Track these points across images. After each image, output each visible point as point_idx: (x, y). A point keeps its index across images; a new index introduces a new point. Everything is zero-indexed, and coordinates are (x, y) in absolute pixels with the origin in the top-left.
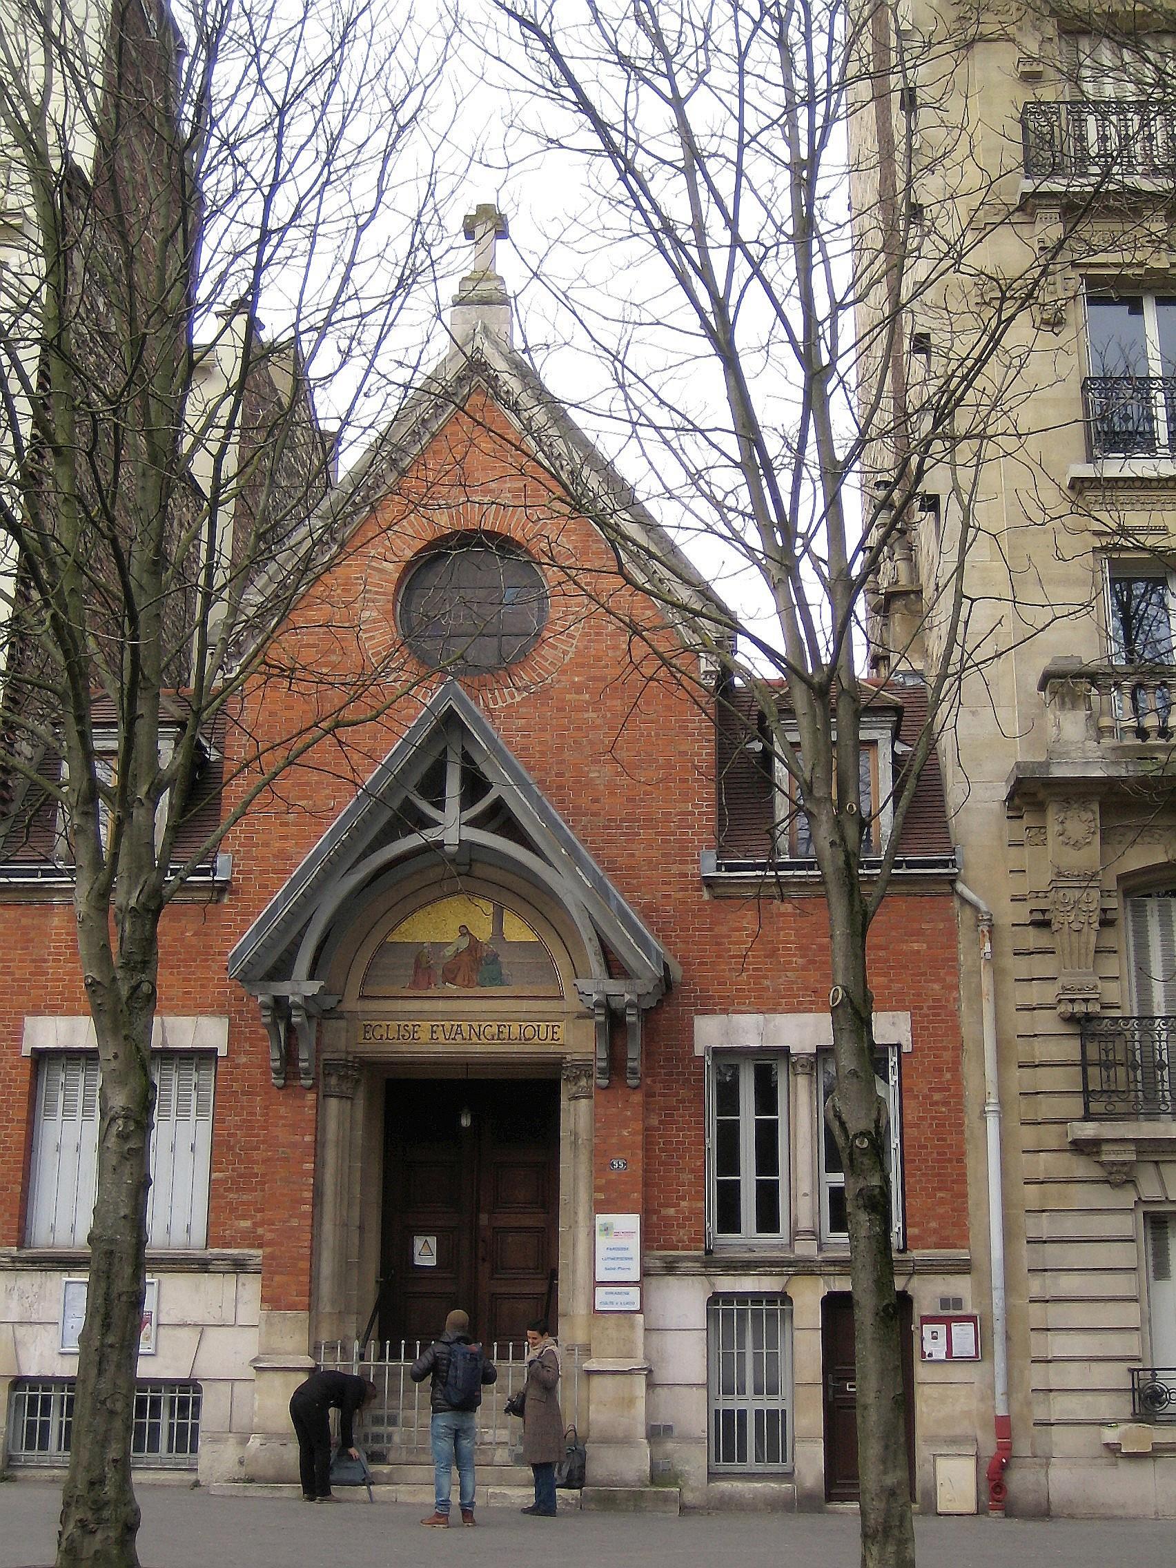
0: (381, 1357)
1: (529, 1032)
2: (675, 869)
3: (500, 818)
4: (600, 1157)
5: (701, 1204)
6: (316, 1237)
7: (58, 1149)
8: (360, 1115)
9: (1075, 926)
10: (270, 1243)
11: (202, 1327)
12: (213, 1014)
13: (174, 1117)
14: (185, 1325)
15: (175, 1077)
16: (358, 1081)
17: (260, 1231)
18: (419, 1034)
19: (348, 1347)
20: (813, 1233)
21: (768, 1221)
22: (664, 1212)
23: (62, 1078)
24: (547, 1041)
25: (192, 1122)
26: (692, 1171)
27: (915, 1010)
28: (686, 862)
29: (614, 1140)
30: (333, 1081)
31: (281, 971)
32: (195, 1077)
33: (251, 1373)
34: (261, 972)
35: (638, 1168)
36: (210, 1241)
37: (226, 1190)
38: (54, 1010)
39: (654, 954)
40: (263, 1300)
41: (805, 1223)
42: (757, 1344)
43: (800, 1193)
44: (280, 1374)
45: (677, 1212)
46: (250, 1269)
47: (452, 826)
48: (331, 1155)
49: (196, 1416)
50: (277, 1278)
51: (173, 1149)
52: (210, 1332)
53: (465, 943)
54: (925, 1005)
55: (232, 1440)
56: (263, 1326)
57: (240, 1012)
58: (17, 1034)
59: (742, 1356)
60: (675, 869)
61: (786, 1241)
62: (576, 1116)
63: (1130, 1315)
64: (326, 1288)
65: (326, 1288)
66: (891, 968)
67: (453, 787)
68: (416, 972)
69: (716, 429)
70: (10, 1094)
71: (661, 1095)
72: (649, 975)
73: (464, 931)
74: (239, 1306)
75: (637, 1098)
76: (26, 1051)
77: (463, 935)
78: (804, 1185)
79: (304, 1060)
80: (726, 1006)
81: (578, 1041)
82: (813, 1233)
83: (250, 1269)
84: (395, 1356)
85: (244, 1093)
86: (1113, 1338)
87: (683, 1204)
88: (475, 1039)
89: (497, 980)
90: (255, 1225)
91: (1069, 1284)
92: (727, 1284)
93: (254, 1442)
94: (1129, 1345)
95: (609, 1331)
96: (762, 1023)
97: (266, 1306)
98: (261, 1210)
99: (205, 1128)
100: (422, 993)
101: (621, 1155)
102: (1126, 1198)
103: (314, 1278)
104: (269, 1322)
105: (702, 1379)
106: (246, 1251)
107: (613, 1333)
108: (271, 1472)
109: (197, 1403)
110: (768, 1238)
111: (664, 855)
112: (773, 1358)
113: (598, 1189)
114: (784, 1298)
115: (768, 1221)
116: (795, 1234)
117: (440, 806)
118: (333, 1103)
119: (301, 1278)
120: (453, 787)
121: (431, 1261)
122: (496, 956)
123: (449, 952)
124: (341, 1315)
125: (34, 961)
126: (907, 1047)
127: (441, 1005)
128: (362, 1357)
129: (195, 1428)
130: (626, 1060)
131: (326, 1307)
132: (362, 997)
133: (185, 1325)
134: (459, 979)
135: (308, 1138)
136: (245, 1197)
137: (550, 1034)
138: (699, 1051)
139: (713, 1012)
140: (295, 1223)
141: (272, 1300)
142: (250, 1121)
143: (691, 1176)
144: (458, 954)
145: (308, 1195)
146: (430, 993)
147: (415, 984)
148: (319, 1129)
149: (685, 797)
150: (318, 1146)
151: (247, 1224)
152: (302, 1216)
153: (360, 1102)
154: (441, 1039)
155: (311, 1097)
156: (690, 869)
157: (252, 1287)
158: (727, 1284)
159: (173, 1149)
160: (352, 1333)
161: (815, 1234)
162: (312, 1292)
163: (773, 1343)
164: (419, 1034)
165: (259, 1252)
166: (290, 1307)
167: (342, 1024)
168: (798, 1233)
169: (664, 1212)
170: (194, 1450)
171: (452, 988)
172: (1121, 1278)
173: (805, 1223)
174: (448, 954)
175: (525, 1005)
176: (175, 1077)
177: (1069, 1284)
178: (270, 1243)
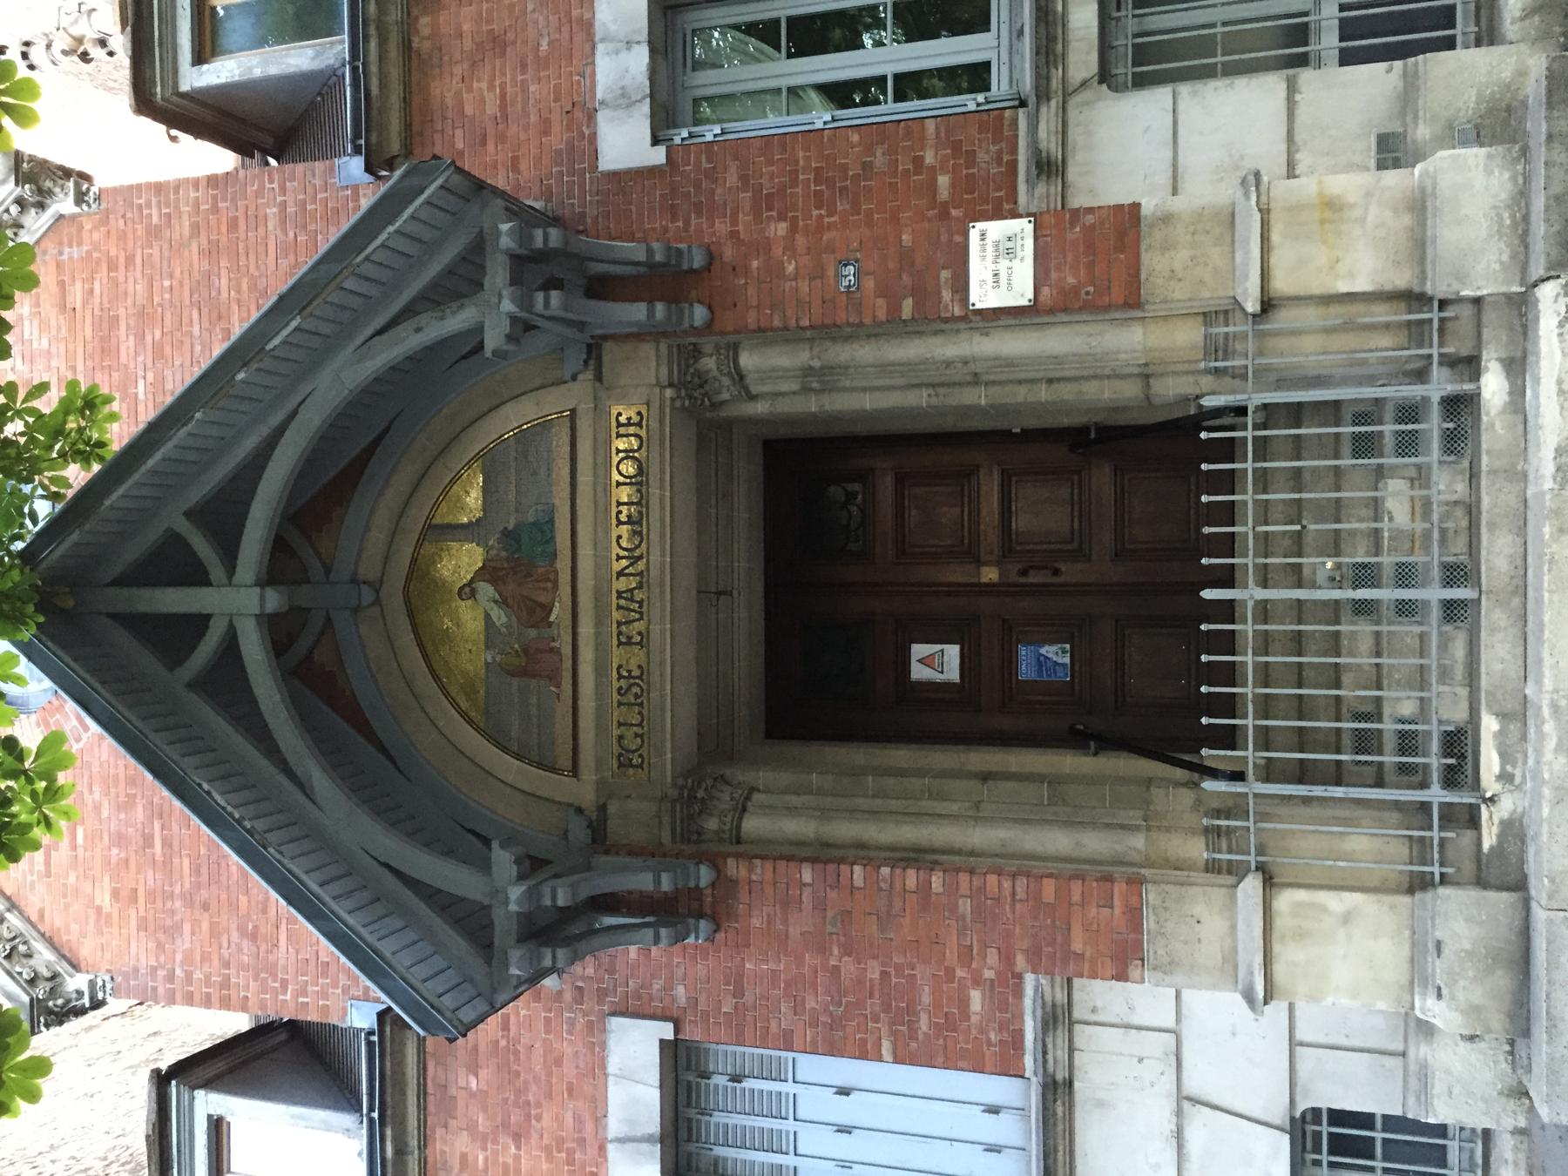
0: (1229, 738)
1: (629, 468)
3: (223, 516)
5: (930, 126)
8: (784, 778)
10: (1007, 958)
11: (1185, 1101)
12: (603, 1046)
13: (789, 1125)
14: (1179, 1135)
16: (723, 779)
17: (989, 974)
18: (633, 665)
19: (1215, 804)
24: (643, 433)
25: (798, 1089)
26: (869, 150)
29: (804, 287)
30: (712, 824)
31: (473, 923)
32: (720, 1080)
33: (1278, 1009)
34: (477, 966)
36: (1009, 1066)
37: (913, 1037)
39: (415, 181)
40: (1121, 976)
44: (1277, 948)
45: (944, 171)
46: (1061, 997)
47: (238, 602)
48: (845, 830)
49: (1365, 1120)
50: (1077, 946)
51: (845, 1130)
52: (1192, 1085)
53: (486, 590)
55: (1421, 1051)
56: (1179, 979)
57: (602, 994)
64: (1095, 843)
65: (1095, 843)
67: (175, 600)
68: (534, 676)
71: (734, 222)
74: (1136, 1021)
77: (473, 594)
79: (658, 881)
80: (581, 114)
83: (1061, 997)
84: (1229, 482)
85: (739, 992)
87: (929, 158)
88: (641, 565)
89: (544, 528)
90: (977, 981)
92: (1082, 58)
93: (1431, 1008)
95: (1178, 266)
96: (610, 46)
97: (1134, 972)
98: (950, 973)
99: (812, 1066)
100: (568, 664)
101: (831, 272)
103: (1074, 870)
104: (1168, 967)
106: (1028, 1002)
107: (1180, 258)
108: (1502, 980)
109: (1338, 1117)
117: (201, 622)
118: (753, 825)
119: (1076, 897)
120: (175, 600)
122: (506, 533)
123: (499, 616)
124: (1151, 822)
127: (586, 629)
128: (1238, 776)
129: (1391, 1122)
130: (651, 265)
132: (575, 771)
133: (1179, 1135)
134: (543, 598)
135: (807, 875)
136: (926, 999)
137: (632, 430)
138: (658, 156)
139: (593, 138)
140: (965, 906)
141: (1124, 958)
142: (788, 984)
144: (503, 602)
145: (912, 878)
146: (567, 650)
147: (554, 677)
149: (259, 220)
150: (824, 854)
151: (976, 999)
152: (952, 890)
153: (762, 777)
155: (733, 868)
157: (1098, 996)
158: (1082, 58)
159: (845, 1130)
160: (1186, 797)
164: (633, 665)
165: (1029, 980)
166: (1135, 916)
167: (613, 808)
170: (1441, 1130)
171: (559, 612)
174: (504, 619)
175: (584, 478)
176: (719, 1118)
178: (1007, 958)
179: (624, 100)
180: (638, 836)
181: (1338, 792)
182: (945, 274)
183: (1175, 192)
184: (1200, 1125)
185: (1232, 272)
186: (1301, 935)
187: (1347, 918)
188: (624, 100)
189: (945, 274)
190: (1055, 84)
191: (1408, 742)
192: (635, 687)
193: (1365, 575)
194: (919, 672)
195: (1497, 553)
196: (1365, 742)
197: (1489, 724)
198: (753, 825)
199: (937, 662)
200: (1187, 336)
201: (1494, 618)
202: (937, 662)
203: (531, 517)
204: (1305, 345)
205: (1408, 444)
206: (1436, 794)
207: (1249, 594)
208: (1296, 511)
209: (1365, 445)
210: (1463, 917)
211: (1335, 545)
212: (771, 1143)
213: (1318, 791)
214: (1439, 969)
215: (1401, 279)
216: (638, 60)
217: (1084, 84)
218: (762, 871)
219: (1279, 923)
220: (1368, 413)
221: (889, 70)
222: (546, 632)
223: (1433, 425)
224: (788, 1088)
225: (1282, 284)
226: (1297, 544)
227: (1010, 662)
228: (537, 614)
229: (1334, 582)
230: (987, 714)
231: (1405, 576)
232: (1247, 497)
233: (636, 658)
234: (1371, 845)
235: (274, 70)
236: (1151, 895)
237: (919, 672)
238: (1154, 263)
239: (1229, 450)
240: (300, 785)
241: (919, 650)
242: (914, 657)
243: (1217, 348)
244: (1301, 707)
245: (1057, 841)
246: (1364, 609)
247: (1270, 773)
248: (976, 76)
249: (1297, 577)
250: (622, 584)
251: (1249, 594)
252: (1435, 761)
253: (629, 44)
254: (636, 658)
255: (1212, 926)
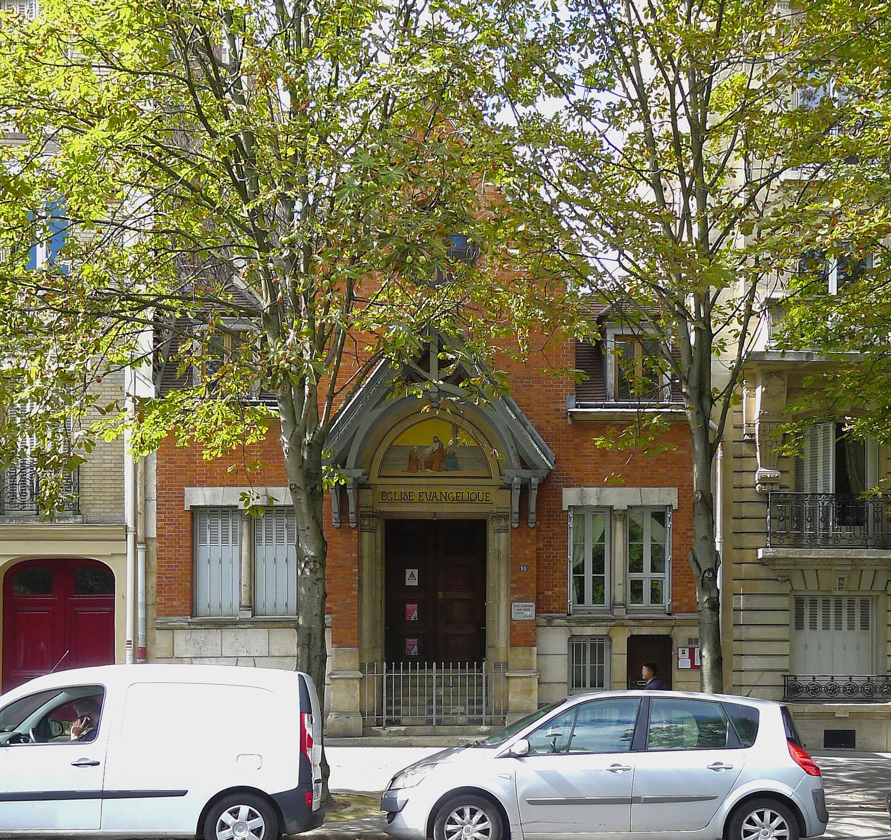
2: (553, 406)
4: (514, 563)
6: (360, 608)
7: (209, 561)
9: (769, 443)
10: (336, 612)
13: (286, 543)
15: (274, 521)
20: (623, 604)
21: (598, 597)
22: (546, 593)
23: (208, 522)
26: (560, 572)
27: (680, 487)
28: (559, 403)
30: (366, 523)
35: (534, 570)
38: (202, 484)
41: (619, 599)
42: (593, 661)
43: (617, 584)
48: (366, 563)
53: (436, 446)
54: (685, 484)
58: (181, 498)
59: (584, 667)
60: (553, 406)
61: (608, 608)
62: (498, 542)
63: (785, 648)
64: (366, 635)
65: (366, 635)
66: (668, 463)
69: (394, 779)
70: (180, 532)
72: (545, 467)
73: (436, 440)
75: (534, 533)
76: (187, 507)
78: (619, 579)
80: (580, 483)
81: (504, 501)
82: (623, 604)
86: (776, 660)
88: (444, 500)
89: (455, 467)
91: (754, 632)
94: (783, 663)
100: (413, 475)
102: (786, 588)
105: (565, 679)
110: (598, 606)
111: (546, 398)
112: (601, 669)
113: (513, 582)
114: (608, 637)
115: (598, 597)
116: (613, 605)
121: (409, 641)
123: (428, 451)
125: (186, 455)
126: (675, 507)
131: (366, 645)
132: (379, 477)
135: (354, 555)
138: (565, 508)
140: (349, 601)
143: (560, 575)
144: (433, 453)
147: (409, 469)
148: (359, 550)
150: (360, 558)
154: (425, 500)
155: (355, 532)
156: (561, 406)
158: (577, 631)
161: (624, 605)
162: (359, 638)
163: (601, 661)
168: (615, 605)
169: (546, 593)
171: (430, 472)
172: (781, 629)
173: (619, 599)
175: (471, 481)
176: (274, 521)
177: (754, 632)
178: (336, 612)
179: (582, 497)
180: (362, 500)
181: (385, 695)
182: (522, 596)
183: (98, 764)
184: (224, 654)
185: (516, 670)
186: (348, 686)
187: (353, 697)
188: (582, 497)
189: (522, 596)
190: (571, 624)
191: (398, 712)
192: (407, 499)
193: (439, 702)
194: (409, 572)
195: (446, 729)
196: (398, 703)
197: (403, 728)
198: (366, 535)
199: (412, 578)
200: (502, 659)
201: (429, 729)
202: (412, 578)
203: (459, 463)
204: (496, 688)
205: (471, 712)
206: (385, 717)
207: (434, 673)
208: (463, 685)
209: (471, 702)
210: (355, 722)
211: (447, 695)
212: (269, 538)
213: (385, 690)
214: (343, 718)
215: (511, 708)
216: (593, 502)
217: (571, 631)
218: (354, 541)
219: (351, 681)
220: (480, 702)
221: (585, 575)
222: (423, 467)
223: (476, 717)
224: (286, 543)
225: (512, 681)
226: (447, 686)
227: (412, 602)
228: (429, 465)
229: (437, 693)
230: (394, 594)
231: (439, 712)
232: (459, 672)
233: (416, 498)
234: (371, 701)
235: (609, 367)
236: (356, 650)
237: (409, 572)
238: (520, 650)
239: (471, 667)
240: (378, 404)
241: (416, 572)
242: (414, 570)
243: (497, 665)
244: (405, 686)
245: (366, 624)
246: (430, 702)
247: (389, 678)
248: (581, 599)
249: (439, 686)
250: (438, 494)
251: (434, 673)
252: (393, 717)
253: (598, 499)
254: (416, 498)
255: (348, 665)
